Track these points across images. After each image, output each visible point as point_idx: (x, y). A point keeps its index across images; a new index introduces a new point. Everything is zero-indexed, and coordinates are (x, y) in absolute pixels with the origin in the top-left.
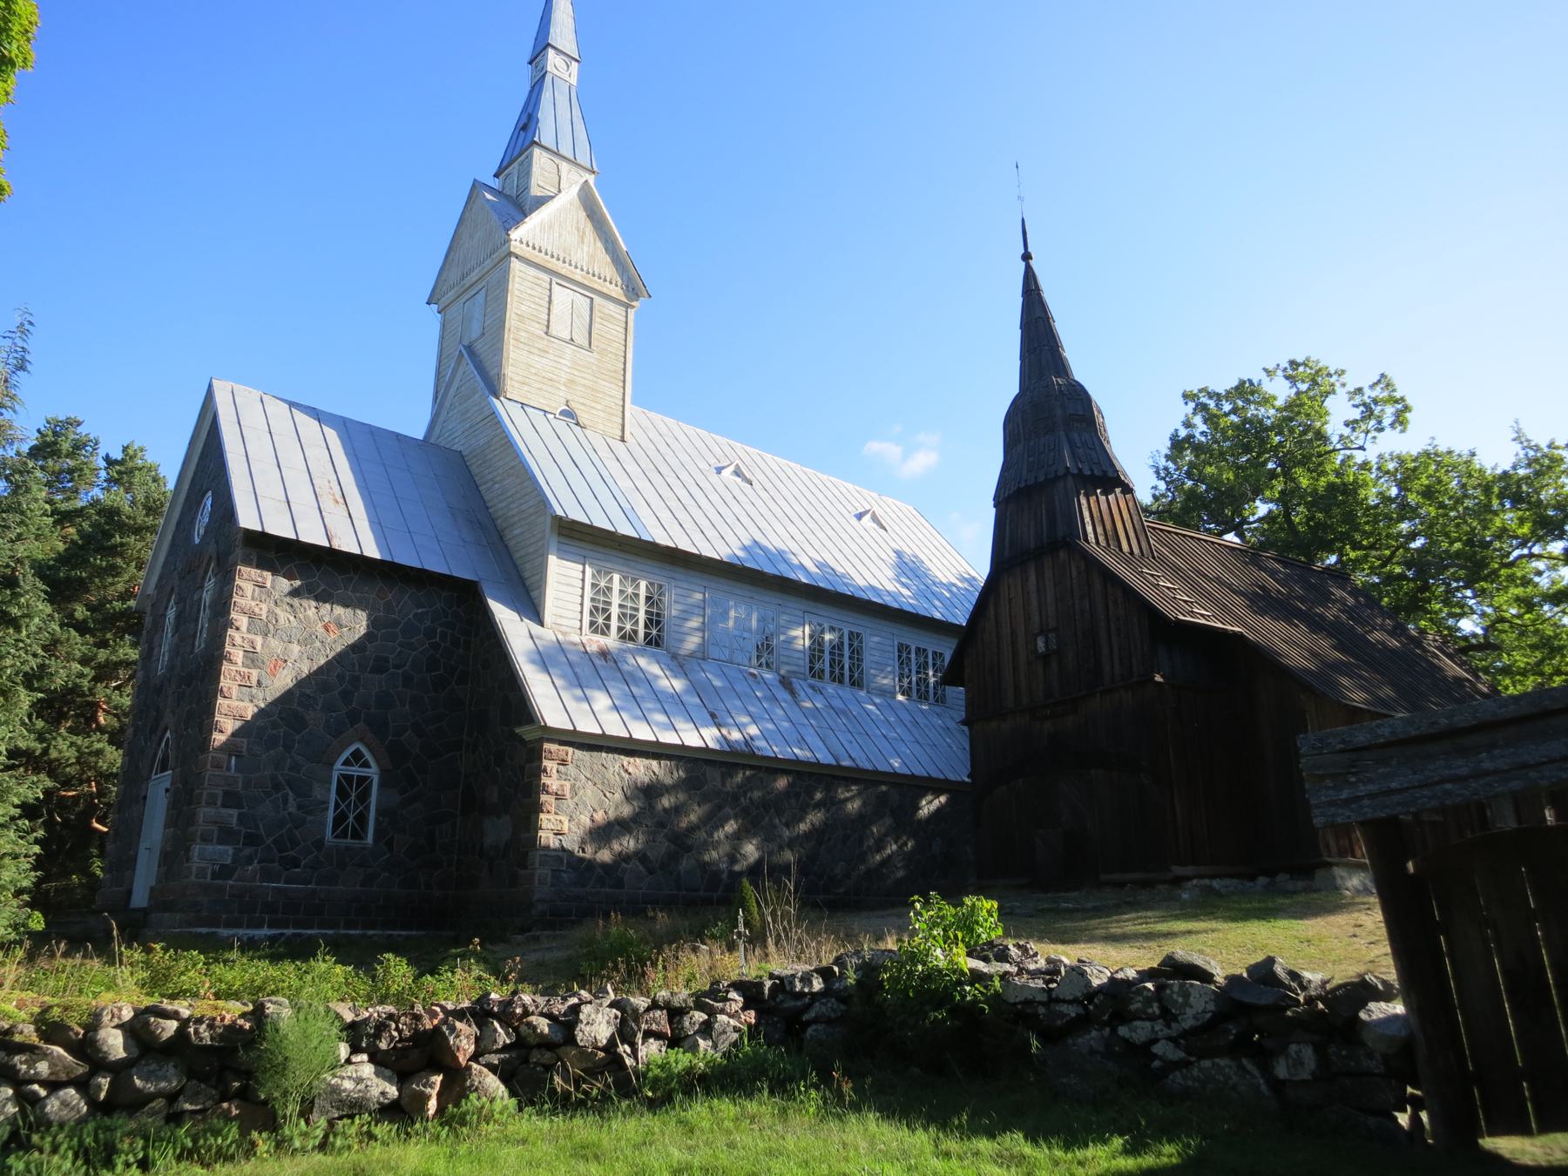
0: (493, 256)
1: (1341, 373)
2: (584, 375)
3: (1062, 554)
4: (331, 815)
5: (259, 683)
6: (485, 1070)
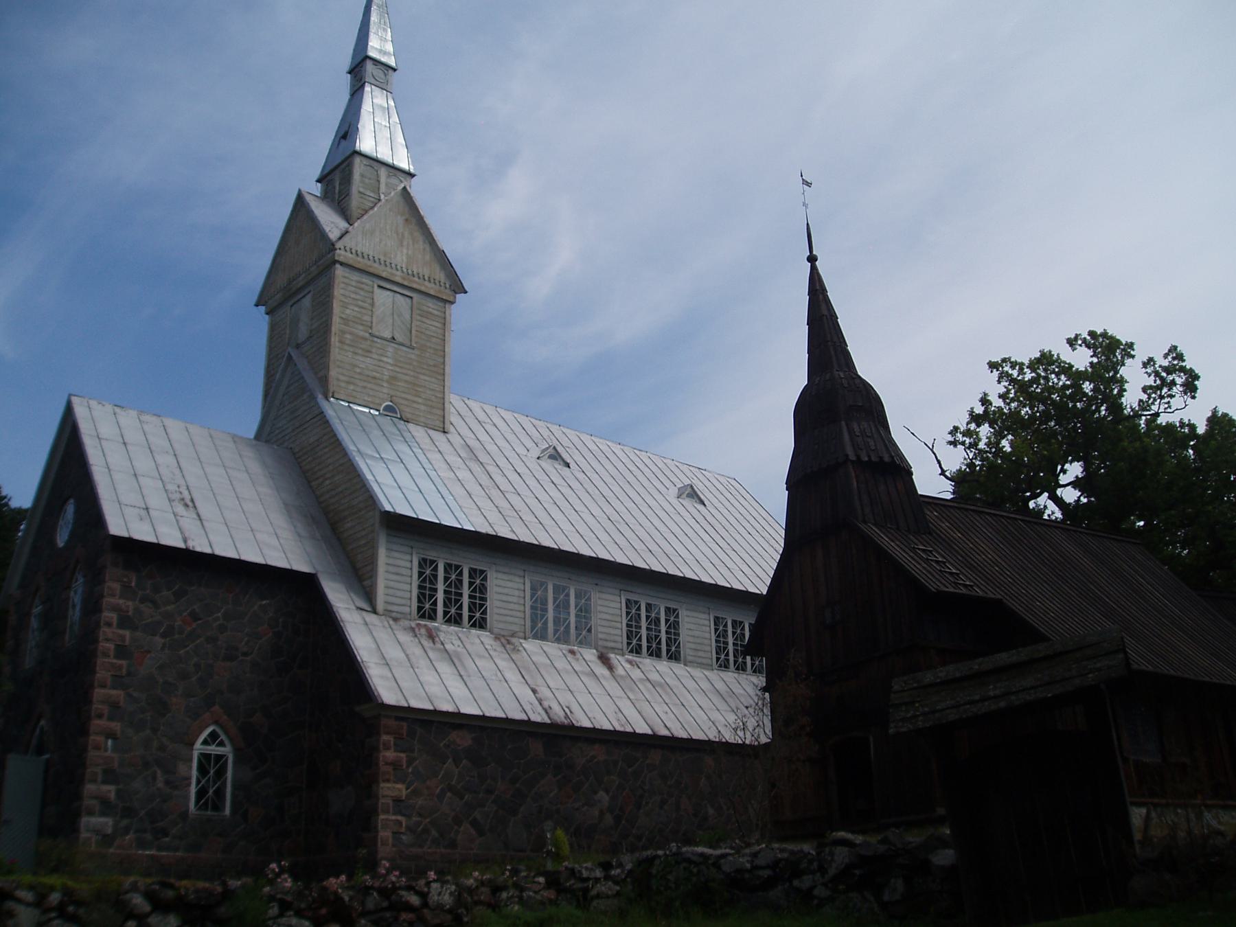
4: (193, 789)
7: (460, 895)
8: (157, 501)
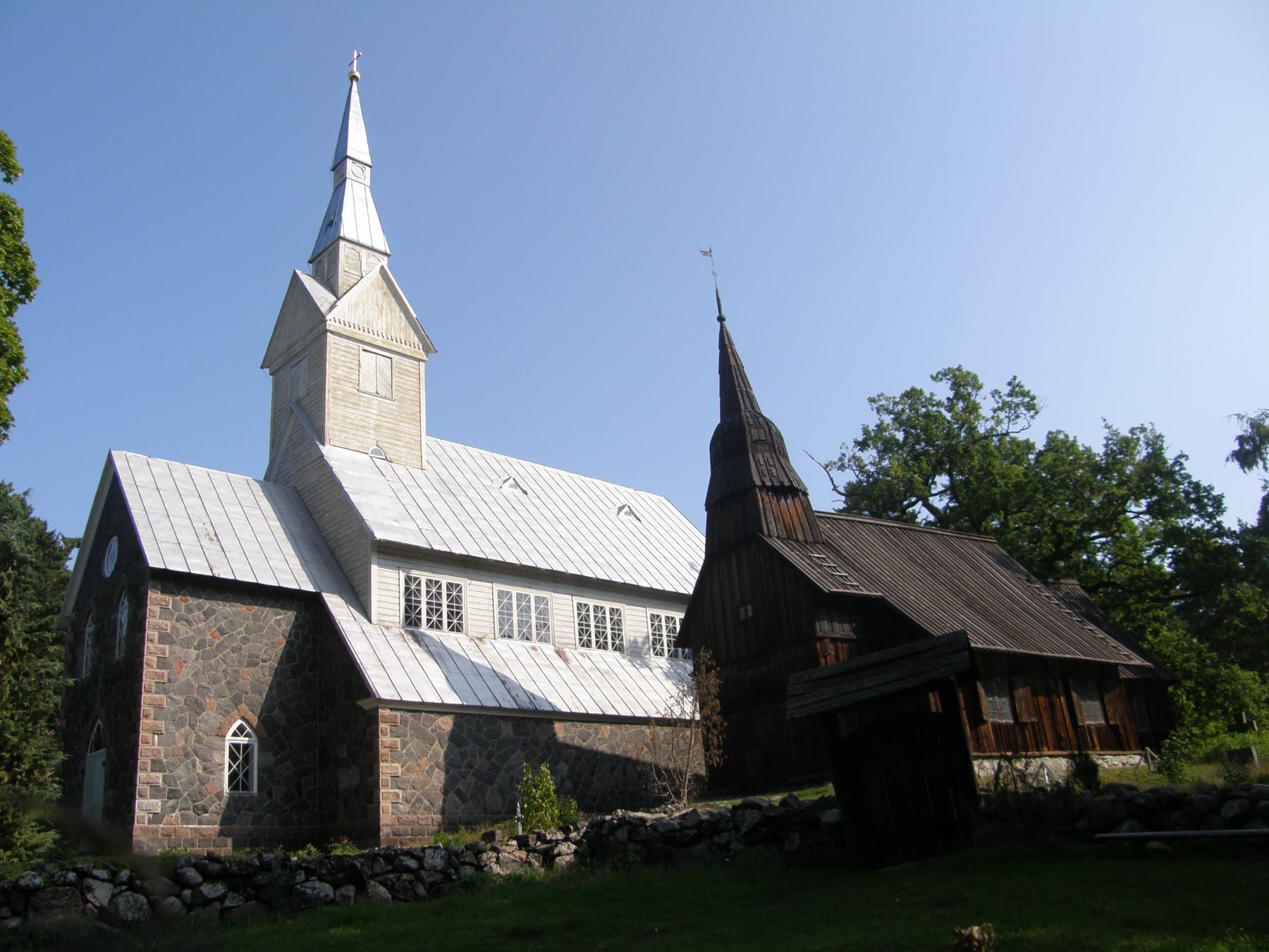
0: (313, 332)
2: (388, 420)
4: (226, 774)
5: (170, 681)
6: (377, 884)
7: (449, 857)
8: (187, 538)
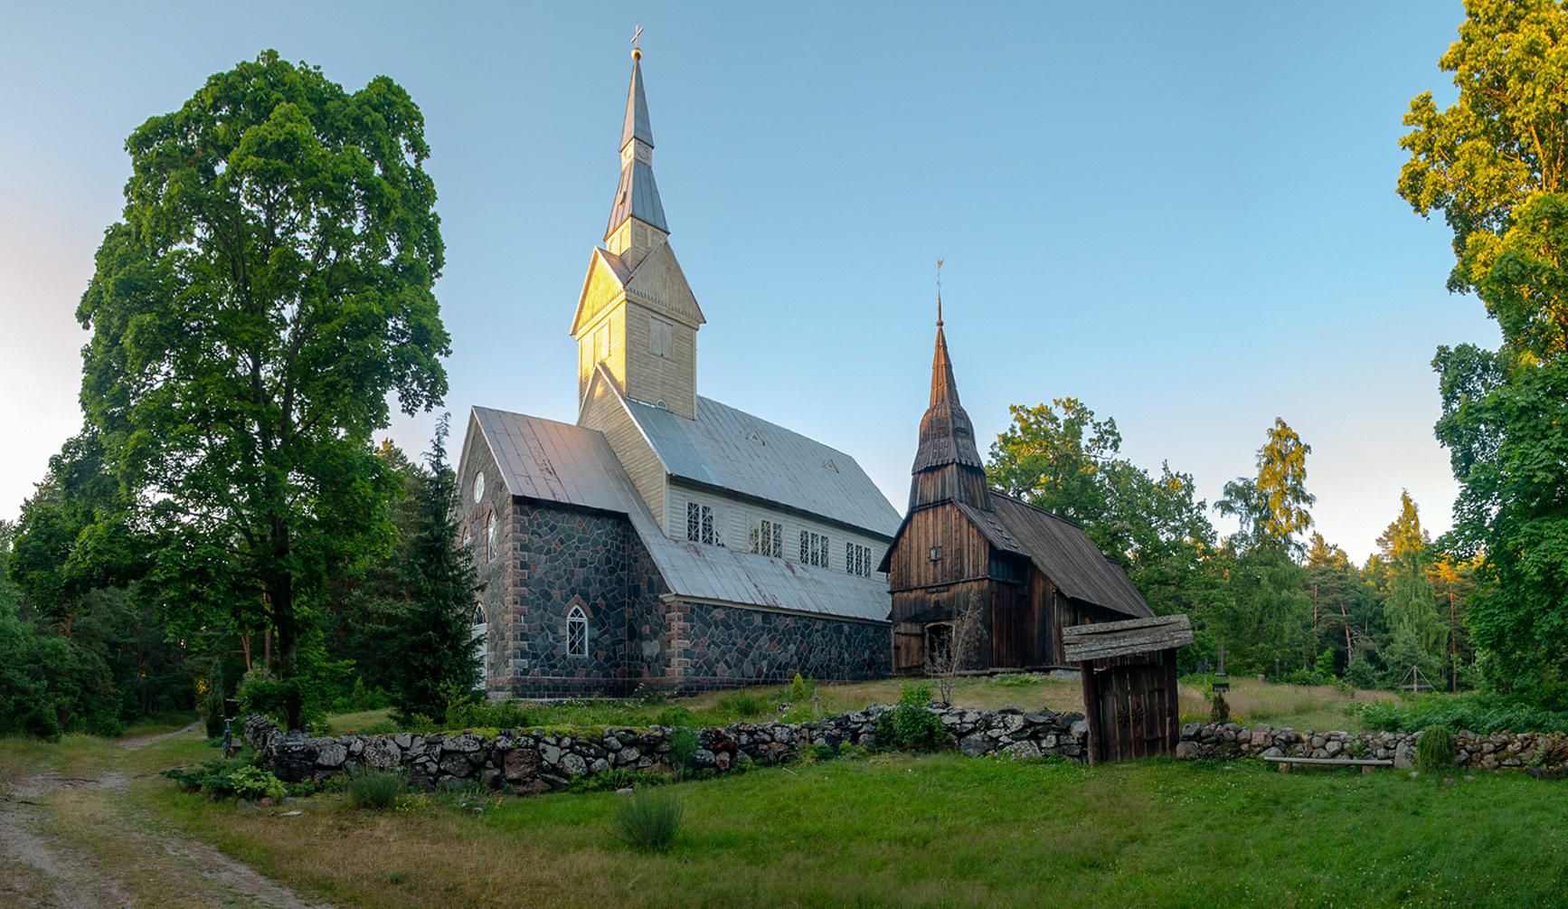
1: (1092, 413)
3: (948, 507)
4: (568, 642)
